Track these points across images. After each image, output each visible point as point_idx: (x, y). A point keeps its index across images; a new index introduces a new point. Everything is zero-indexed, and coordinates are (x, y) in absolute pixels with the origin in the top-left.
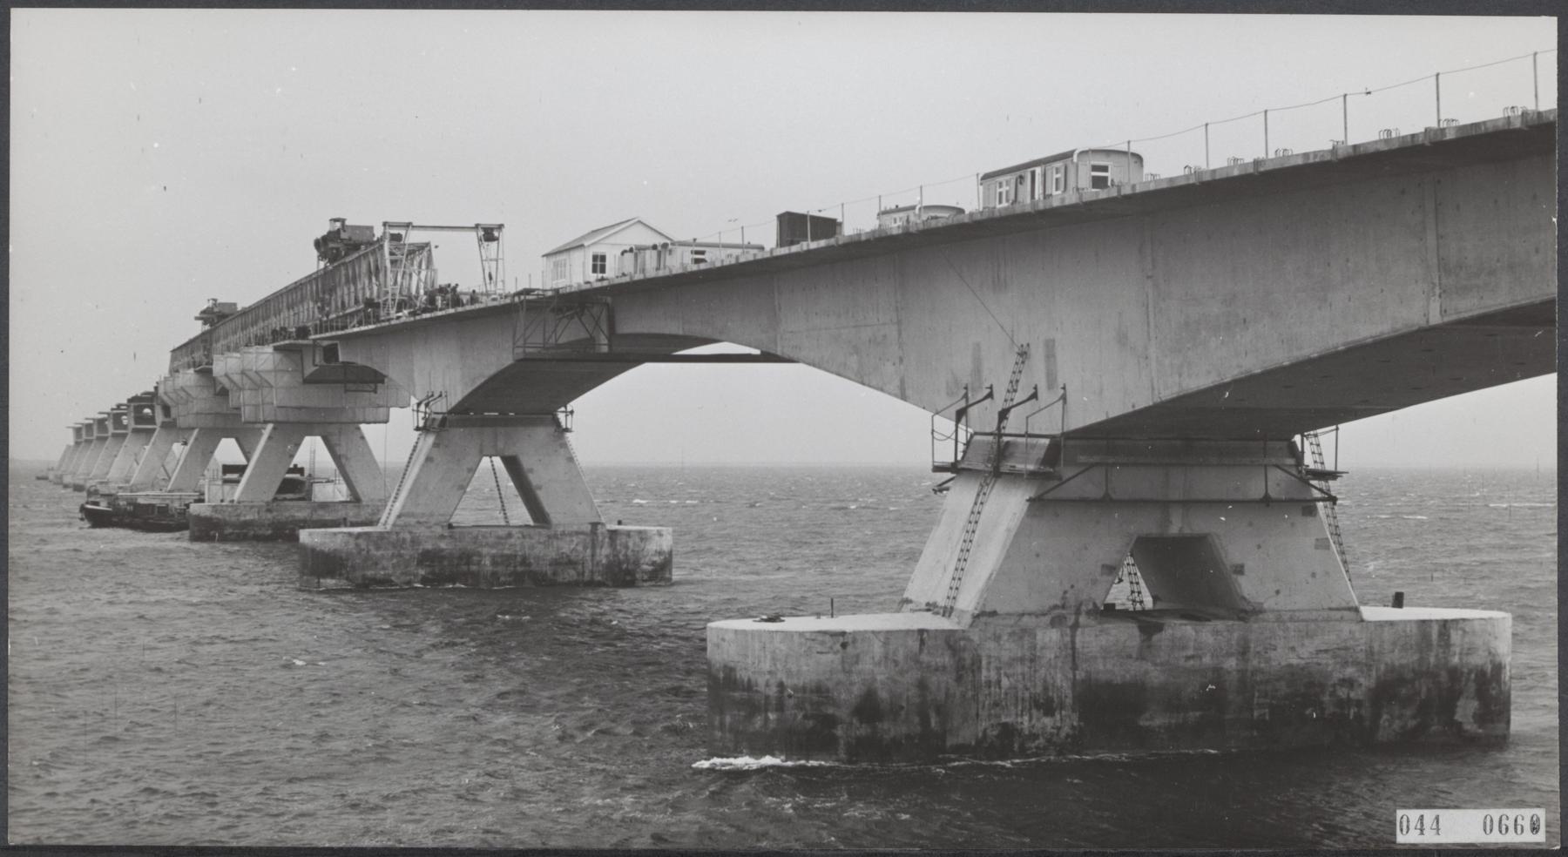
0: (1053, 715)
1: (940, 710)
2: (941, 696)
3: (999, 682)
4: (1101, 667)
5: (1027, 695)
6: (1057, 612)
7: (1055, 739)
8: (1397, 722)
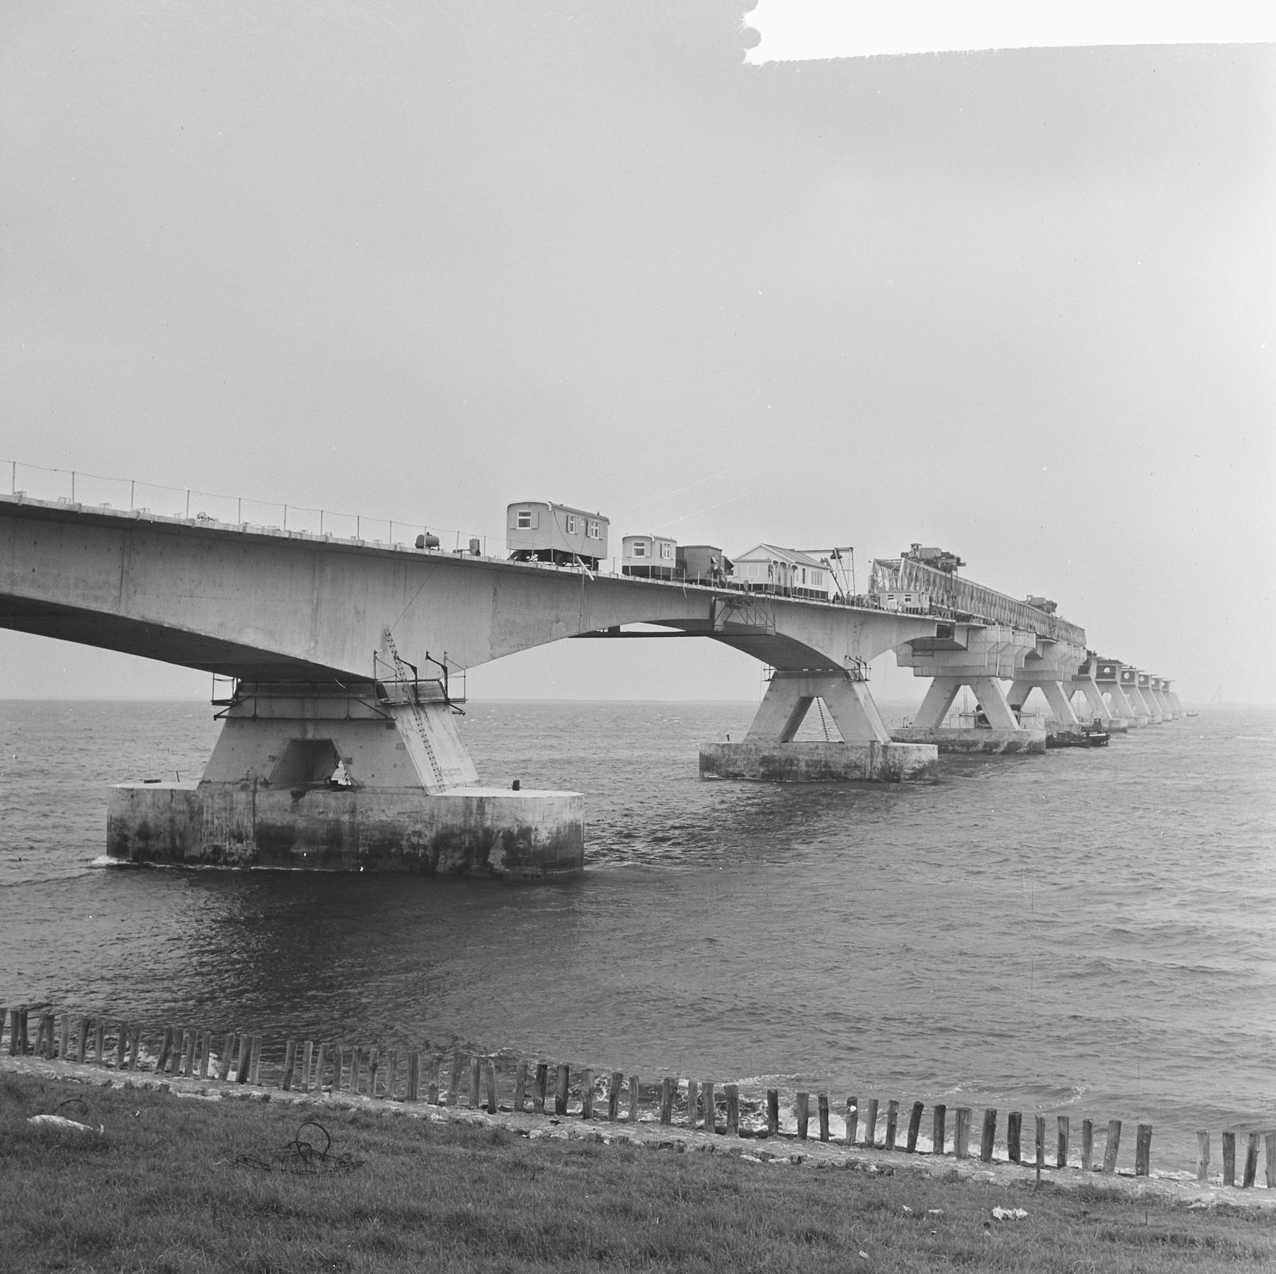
0: (242, 843)
1: (181, 835)
2: (182, 828)
3: (213, 822)
4: (269, 816)
5: (228, 830)
6: (244, 782)
7: (243, 856)
8: (450, 861)
